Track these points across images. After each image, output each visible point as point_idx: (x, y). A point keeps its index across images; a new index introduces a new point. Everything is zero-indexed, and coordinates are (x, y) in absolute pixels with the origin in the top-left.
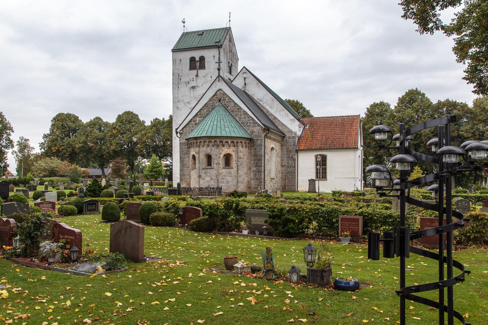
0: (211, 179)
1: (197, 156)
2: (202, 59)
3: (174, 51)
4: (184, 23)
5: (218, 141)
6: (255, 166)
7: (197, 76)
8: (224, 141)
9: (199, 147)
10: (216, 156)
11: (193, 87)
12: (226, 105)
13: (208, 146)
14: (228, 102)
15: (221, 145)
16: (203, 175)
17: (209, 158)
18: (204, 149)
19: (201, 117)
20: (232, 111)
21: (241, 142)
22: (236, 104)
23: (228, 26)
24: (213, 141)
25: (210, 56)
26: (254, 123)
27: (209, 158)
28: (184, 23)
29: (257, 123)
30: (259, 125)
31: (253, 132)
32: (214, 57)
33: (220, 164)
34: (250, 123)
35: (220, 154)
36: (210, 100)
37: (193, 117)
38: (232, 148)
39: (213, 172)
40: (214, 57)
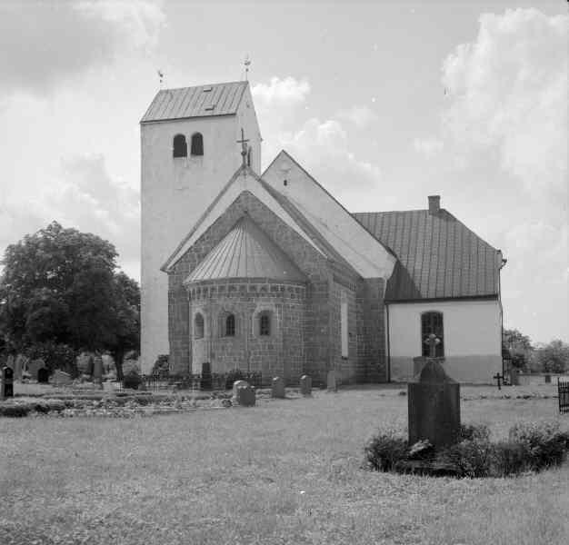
35: (252, 311)
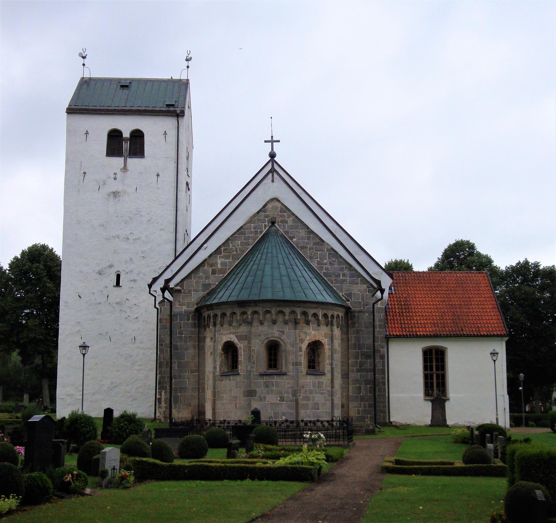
0: (282, 399)
1: (240, 345)
2: (138, 136)
3: (71, 111)
4: (84, 58)
5: (299, 311)
6: (358, 371)
7: (125, 168)
8: (311, 312)
9: (250, 324)
10: (293, 345)
11: (115, 194)
12: (287, 232)
13: (274, 322)
14: (292, 227)
15: (302, 321)
16: (260, 390)
17: (273, 349)
18: (264, 328)
19: (228, 257)
20: (302, 248)
21: (315, 315)
22: (312, 232)
23: (184, 77)
24: (287, 310)
25: (154, 129)
26: (352, 276)
27: (273, 349)
28: (84, 58)
29: (360, 275)
30: (365, 281)
31: (350, 295)
32: (165, 133)
33: (300, 364)
34: (344, 275)
35: (302, 341)
36: (251, 220)
37: (210, 256)
38: (324, 330)
39: (285, 383)
40: (165, 133)
